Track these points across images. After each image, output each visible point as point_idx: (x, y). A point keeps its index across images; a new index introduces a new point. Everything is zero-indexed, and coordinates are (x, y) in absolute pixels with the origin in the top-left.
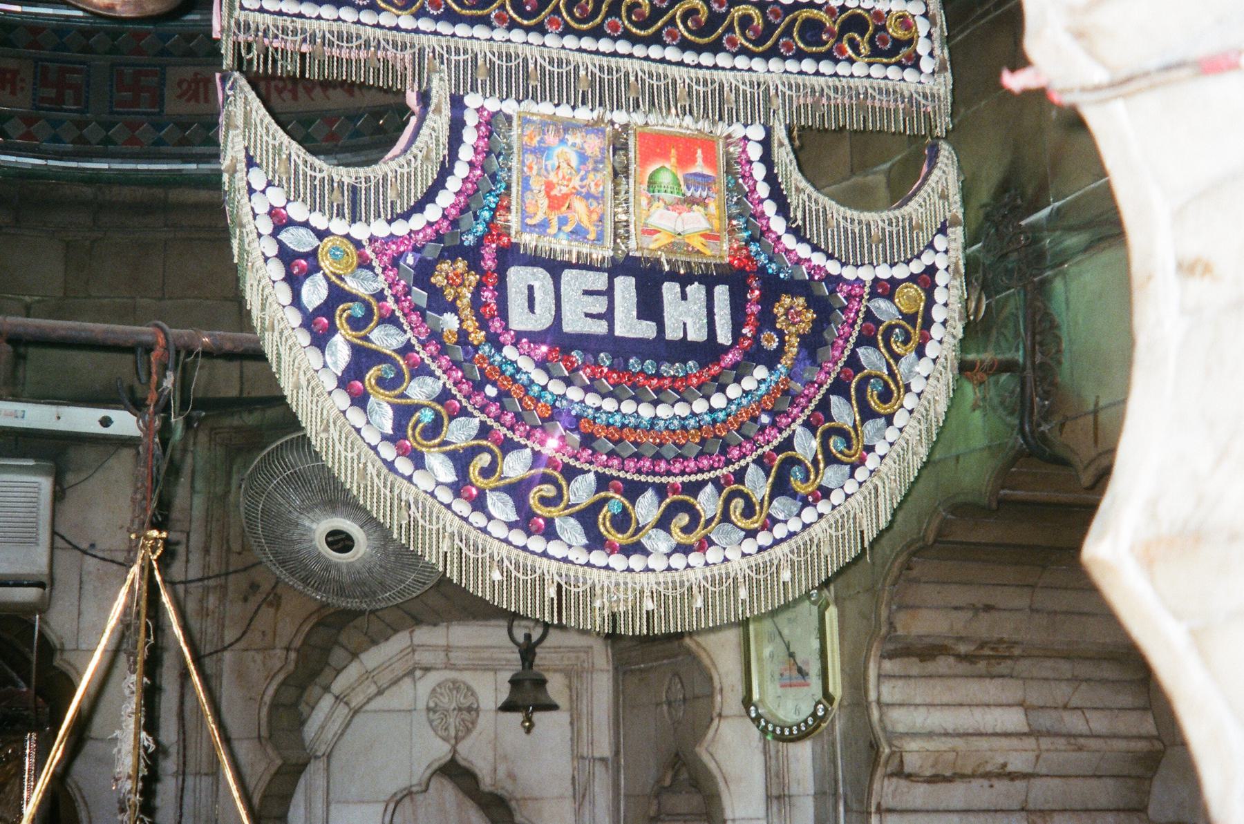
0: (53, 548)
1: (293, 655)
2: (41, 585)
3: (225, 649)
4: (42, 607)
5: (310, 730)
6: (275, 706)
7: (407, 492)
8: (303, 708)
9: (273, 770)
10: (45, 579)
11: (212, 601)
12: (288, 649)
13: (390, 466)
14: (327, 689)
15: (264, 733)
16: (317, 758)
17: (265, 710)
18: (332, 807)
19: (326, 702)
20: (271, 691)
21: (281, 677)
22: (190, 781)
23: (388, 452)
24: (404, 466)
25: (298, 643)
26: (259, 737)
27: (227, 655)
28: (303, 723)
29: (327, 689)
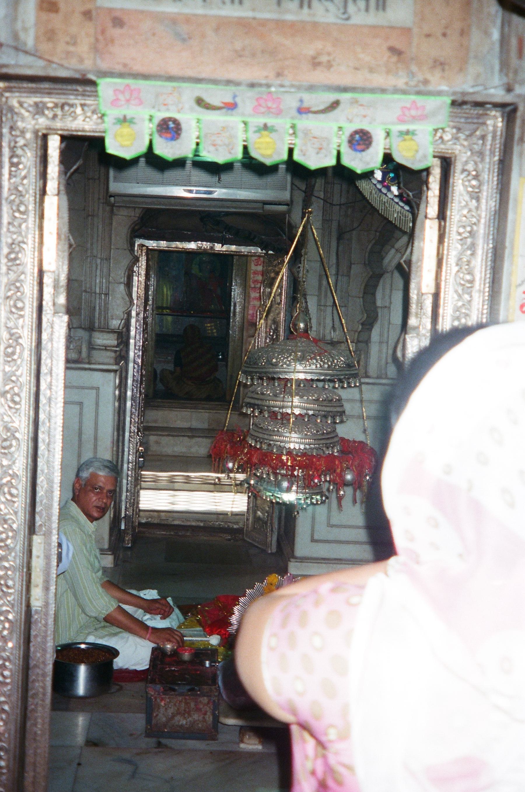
0: (292, 189)
1: (378, 234)
2: (287, 205)
3: (353, 230)
4: (289, 212)
5: (386, 261)
6: (371, 252)
7: (385, 199)
8: (383, 254)
9: (369, 276)
10: (289, 203)
11: (350, 211)
12: (376, 231)
13: (380, 190)
14: (393, 247)
15: (367, 262)
16: (388, 272)
17: (367, 254)
18: (394, 292)
19: (393, 251)
20: (369, 247)
21: (374, 242)
22: (340, 278)
23: (379, 186)
24: (384, 190)
25: (380, 229)
26: (365, 263)
27: (354, 232)
28: (383, 259)
29: (393, 247)
